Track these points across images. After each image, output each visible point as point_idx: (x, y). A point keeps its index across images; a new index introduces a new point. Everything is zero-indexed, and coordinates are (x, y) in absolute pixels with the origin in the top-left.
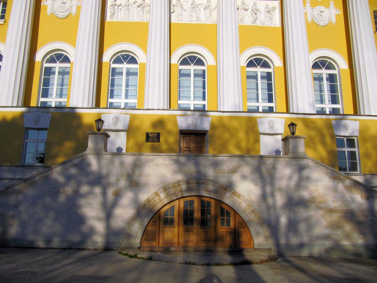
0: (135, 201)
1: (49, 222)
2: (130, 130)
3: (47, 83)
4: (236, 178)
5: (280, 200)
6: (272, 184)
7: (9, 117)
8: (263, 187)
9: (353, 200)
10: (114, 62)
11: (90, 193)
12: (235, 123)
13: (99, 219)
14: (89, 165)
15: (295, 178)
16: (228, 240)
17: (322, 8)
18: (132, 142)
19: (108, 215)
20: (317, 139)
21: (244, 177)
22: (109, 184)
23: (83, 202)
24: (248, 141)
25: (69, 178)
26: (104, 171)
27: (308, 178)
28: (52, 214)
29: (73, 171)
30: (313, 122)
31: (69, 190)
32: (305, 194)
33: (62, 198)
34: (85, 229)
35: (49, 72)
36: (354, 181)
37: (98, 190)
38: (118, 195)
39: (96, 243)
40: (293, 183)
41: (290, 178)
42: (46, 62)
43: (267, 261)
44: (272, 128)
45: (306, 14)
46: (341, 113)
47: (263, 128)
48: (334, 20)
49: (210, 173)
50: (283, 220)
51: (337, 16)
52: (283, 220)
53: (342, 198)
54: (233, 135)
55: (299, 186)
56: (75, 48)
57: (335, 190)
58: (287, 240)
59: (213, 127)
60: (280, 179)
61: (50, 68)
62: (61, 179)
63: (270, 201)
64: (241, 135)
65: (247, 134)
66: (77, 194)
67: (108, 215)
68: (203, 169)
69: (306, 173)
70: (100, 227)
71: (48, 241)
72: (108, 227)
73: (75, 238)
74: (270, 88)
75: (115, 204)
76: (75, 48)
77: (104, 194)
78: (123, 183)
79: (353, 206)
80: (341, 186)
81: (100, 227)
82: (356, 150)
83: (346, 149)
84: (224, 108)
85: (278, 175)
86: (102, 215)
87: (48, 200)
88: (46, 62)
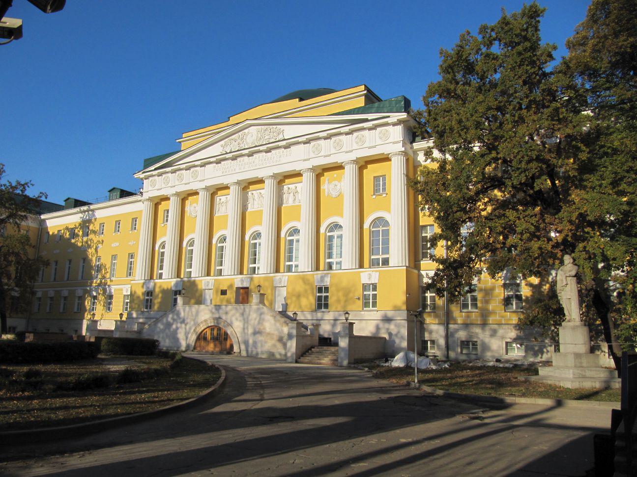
3: (330, 247)
4: (234, 319)
5: (250, 331)
6: (247, 322)
10: (329, 231)
13: (183, 339)
14: (180, 314)
19: (187, 338)
20: (309, 292)
21: (237, 319)
22: (187, 323)
35: (331, 238)
37: (183, 325)
40: (256, 322)
42: (328, 232)
43: (472, 324)
49: (224, 317)
52: (251, 341)
53: (278, 329)
56: (390, 213)
60: (251, 320)
61: (255, 244)
63: (246, 331)
66: (177, 328)
67: (187, 338)
76: (390, 213)
83: (371, 293)
86: (185, 338)
88: (328, 232)
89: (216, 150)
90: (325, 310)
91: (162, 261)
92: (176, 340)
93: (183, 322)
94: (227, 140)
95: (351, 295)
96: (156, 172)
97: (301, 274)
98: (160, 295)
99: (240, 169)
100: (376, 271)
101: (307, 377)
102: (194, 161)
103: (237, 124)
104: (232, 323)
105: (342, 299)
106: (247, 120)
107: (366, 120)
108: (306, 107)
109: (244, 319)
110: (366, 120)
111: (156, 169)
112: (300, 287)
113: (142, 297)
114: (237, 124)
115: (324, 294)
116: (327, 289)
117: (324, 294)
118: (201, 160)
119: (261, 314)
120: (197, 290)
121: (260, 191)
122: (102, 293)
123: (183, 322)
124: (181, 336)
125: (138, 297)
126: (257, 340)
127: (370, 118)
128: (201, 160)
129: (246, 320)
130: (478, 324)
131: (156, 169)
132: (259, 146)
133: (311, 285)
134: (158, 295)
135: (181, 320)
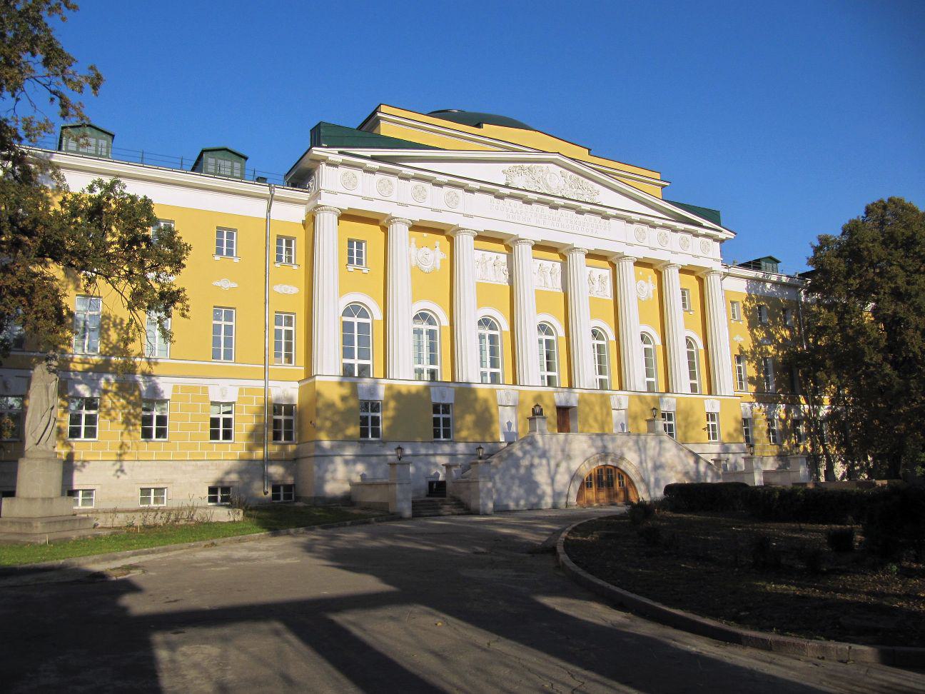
0: (568, 469)
1: (515, 488)
2: (517, 406)
4: (625, 450)
5: (650, 465)
6: (645, 454)
7: (414, 390)
8: (640, 456)
9: (689, 464)
11: (541, 464)
12: (593, 399)
13: (547, 484)
14: (537, 442)
15: (657, 449)
16: (622, 496)
17: (428, 250)
18: (519, 415)
19: (553, 480)
21: (630, 449)
23: (535, 471)
24: (602, 414)
25: (525, 453)
26: (547, 447)
27: (664, 449)
28: (517, 482)
29: (528, 447)
30: (644, 397)
31: (525, 462)
32: (663, 460)
33: (522, 471)
34: (539, 492)
36: (388, 443)
37: (544, 461)
38: (558, 465)
39: (546, 504)
41: (654, 448)
44: (443, 397)
45: (410, 256)
46: (457, 381)
47: (614, 403)
48: (438, 266)
50: (652, 479)
51: (442, 261)
52: (652, 479)
54: (592, 409)
55: (659, 454)
57: (679, 457)
58: (655, 493)
59: (579, 402)
62: (520, 454)
63: (644, 465)
64: (597, 409)
65: (601, 408)
67: (553, 480)
68: (606, 443)
69: (663, 445)
70: (548, 490)
71: (517, 505)
72: (554, 490)
73: (533, 500)
74: (289, 347)
75: (556, 472)
77: (549, 465)
78: (560, 456)
79: (688, 467)
80: (682, 454)
81: (548, 490)
82: (379, 414)
84: (441, 377)
85: (648, 446)
86: (549, 481)
87: (513, 471)
89: (494, 173)
90: (373, 439)
91: (691, 365)
92: (531, 485)
93: (544, 455)
94: (518, 165)
95: (690, 419)
96: (376, 165)
97: (585, 391)
98: (392, 404)
101: (211, 564)
102: (633, 212)
103: (544, 152)
104: (623, 454)
105: (683, 424)
106: (558, 153)
107: (700, 225)
108: (646, 179)
109: (639, 449)
110: (700, 225)
111: (374, 158)
112: (637, 407)
113: (339, 404)
114: (544, 152)
115: (371, 414)
116: (446, 408)
117: (371, 414)
118: (619, 209)
119: (661, 442)
120: (476, 399)
121: (591, 268)
122: (114, 389)
123: (544, 455)
124: (541, 477)
125: (331, 406)
126: (659, 477)
128: (619, 209)
129: (642, 449)
131: (374, 158)
132: (527, 191)
133: (647, 403)
134: (386, 403)
135: (540, 452)
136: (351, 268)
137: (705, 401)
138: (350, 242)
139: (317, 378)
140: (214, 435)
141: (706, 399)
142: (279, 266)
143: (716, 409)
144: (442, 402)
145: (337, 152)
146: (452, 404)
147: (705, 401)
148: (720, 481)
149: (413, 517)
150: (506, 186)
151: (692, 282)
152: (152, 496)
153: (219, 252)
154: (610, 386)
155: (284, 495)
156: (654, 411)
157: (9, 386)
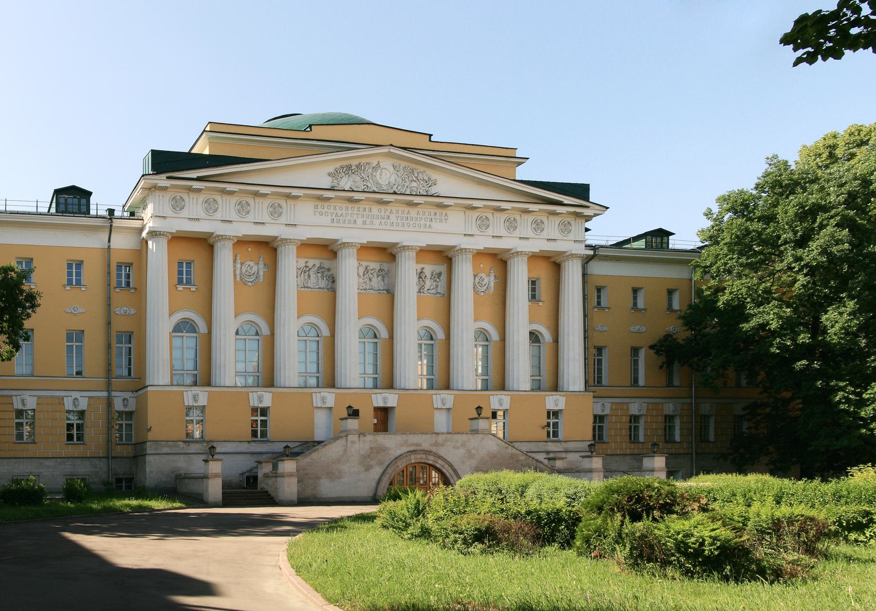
44: (24, 404)
99: (364, 223)
100: (508, 395)
106: (391, 145)
111: (199, 179)
127: (566, 202)
130: (617, 455)
131: (199, 179)
136: (180, 288)
137: (547, 398)
138: (180, 264)
139: (149, 388)
140: (70, 437)
141: (548, 396)
142: (118, 291)
143: (561, 406)
144: (261, 406)
145: (165, 178)
146: (393, 408)
147: (434, 397)
148: (148, 475)
149: (298, 503)
150: (332, 189)
151: (543, 274)
152: (124, 484)
153: (180, 282)
154: (563, 388)
155: (126, 486)
156: (479, 409)
157: (25, 403)
